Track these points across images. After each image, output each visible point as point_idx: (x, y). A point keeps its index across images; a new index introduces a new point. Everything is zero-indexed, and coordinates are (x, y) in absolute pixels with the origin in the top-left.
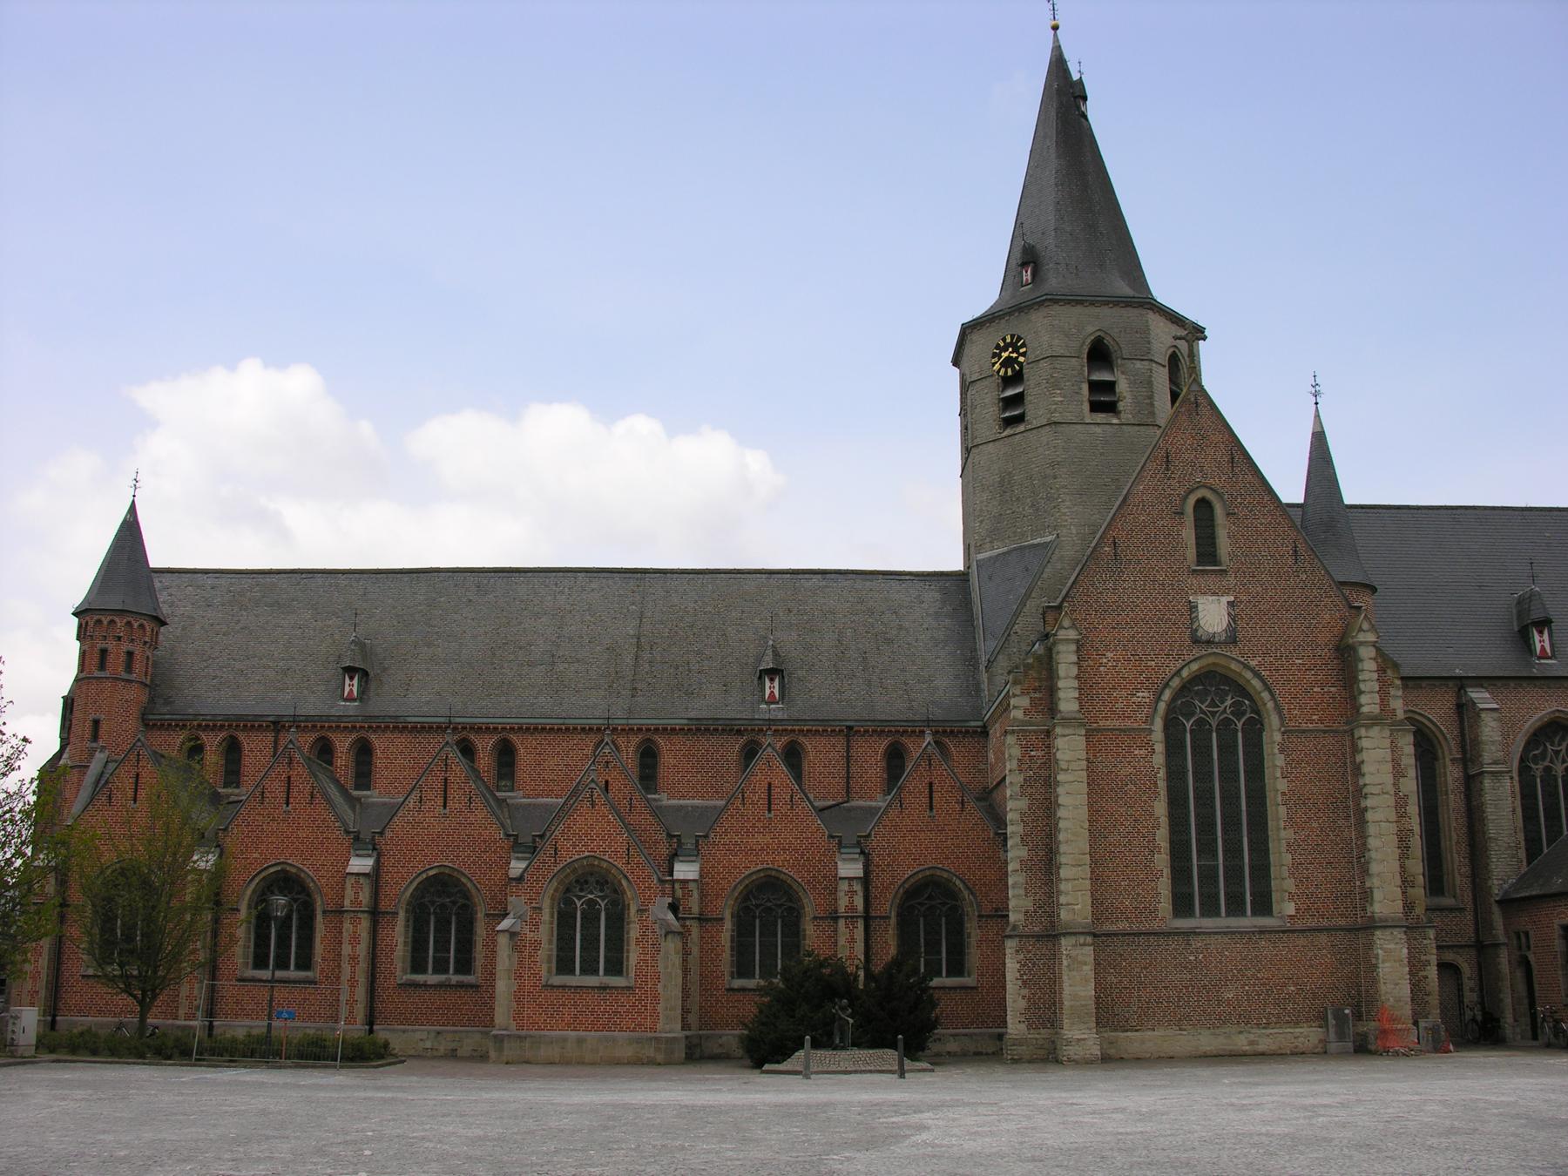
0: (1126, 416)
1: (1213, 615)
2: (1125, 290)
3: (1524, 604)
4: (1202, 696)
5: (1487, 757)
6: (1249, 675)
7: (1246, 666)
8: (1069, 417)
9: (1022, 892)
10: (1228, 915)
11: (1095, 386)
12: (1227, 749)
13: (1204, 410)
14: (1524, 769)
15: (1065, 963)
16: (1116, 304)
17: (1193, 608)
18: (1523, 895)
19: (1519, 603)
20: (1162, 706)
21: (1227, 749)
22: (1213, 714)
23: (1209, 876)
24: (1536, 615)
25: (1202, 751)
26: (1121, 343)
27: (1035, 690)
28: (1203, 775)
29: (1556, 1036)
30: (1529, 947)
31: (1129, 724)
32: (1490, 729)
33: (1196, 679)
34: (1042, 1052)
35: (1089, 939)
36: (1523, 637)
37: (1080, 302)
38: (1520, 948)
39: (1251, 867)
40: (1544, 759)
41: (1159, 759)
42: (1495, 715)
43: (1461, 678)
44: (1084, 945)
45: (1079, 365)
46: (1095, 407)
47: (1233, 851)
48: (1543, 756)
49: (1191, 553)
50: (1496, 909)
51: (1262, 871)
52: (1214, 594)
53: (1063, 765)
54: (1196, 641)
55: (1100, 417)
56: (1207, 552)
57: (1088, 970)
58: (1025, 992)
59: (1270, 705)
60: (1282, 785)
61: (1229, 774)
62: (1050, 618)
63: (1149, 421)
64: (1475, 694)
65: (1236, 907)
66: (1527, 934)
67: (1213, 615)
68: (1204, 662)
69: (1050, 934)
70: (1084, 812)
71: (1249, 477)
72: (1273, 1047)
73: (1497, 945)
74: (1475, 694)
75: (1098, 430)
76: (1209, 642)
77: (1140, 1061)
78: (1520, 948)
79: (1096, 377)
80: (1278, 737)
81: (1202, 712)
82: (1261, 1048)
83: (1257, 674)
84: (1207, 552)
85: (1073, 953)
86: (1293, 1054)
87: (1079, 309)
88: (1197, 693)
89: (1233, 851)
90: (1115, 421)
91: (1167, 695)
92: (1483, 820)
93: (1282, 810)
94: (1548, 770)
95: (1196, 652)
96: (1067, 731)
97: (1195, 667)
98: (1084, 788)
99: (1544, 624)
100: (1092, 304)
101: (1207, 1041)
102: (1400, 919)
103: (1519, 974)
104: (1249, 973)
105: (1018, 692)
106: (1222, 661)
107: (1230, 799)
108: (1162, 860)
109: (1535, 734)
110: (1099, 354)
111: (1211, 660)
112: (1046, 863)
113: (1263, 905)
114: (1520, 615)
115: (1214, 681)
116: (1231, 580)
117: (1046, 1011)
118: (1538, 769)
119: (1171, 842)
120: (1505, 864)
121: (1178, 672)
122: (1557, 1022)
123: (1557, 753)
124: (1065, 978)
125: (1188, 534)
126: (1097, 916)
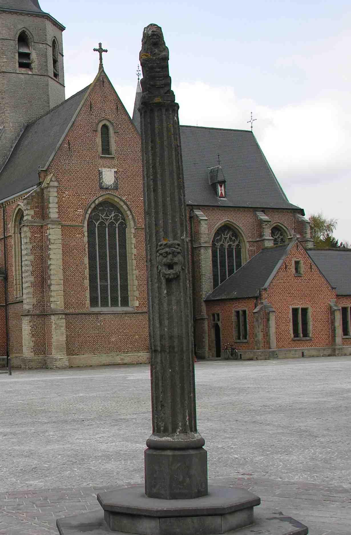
0: (35, 71)
1: (109, 177)
2: (35, 9)
3: (213, 174)
4: (102, 211)
5: (202, 240)
6: (122, 203)
7: (121, 200)
8: (9, 69)
9: (32, 296)
10: (101, 306)
11: (22, 55)
12: (112, 235)
13: (106, 85)
14: (214, 245)
15: (54, 326)
16: (32, 15)
17: (100, 173)
18: (218, 298)
19: (211, 172)
20: (87, 216)
21: (112, 235)
22: (107, 220)
23: (104, 289)
24: (220, 179)
25: (102, 236)
26: (33, 34)
27: (36, 207)
28: (102, 246)
29: (232, 355)
30: (219, 320)
31: (74, 223)
32: (204, 228)
33: (100, 204)
34: (40, 365)
35: (64, 316)
36: (214, 188)
37: (16, 13)
38: (214, 320)
39: (121, 286)
40: (221, 241)
41: (86, 239)
42: (206, 222)
43: (192, 205)
44: (62, 319)
45: (14, 43)
46: (22, 65)
47: (114, 279)
48: (220, 240)
49: (100, 149)
50: (203, 304)
51: (125, 288)
52: (109, 167)
53: (52, 241)
54: (101, 188)
55: (23, 70)
56: (106, 149)
57: (63, 329)
58: (33, 339)
59: (130, 217)
60: (135, 251)
61: (112, 247)
62: (42, 175)
63: (44, 73)
64: (198, 213)
65: (114, 303)
66: (218, 315)
67: (109, 177)
68: (104, 197)
69: (42, 314)
70: (60, 262)
71: (124, 116)
72: (130, 361)
73: (203, 319)
74: (198, 213)
75: (22, 76)
76: (107, 189)
77: (79, 367)
78: (214, 320)
79: (21, 50)
80: (133, 231)
81: (102, 219)
82: (125, 362)
83: (125, 204)
84: (106, 149)
85: (57, 322)
86: (137, 364)
87: (15, 16)
88: (100, 210)
89: (114, 279)
90: (30, 73)
91: (89, 212)
92: (199, 267)
93: (134, 262)
94: (230, 246)
95: (102, 193)
96: (53, 227)
97: (101, 199)
98: (61, 252)
99: (222, 183)
100: (21, 14)
101: (105, 359)
102: (62, 310)
103: (213, 331)
104: (121, 331)
105: (29, 208)
106: (112, 197)
107: (113, 257)
108: (87, 282)
109: (218, 230)
110: (23, 39)
111: (107, 196)
112: (42, 282)
113: (125, 302)
114: (212, 177)
115: (107, 205)
116: (116, 162)
117: (42, 345)
118: (218, 245)
119: (90, 275)
120: (207, 287)
121: (94, 202)
122: (233, 349)
123: (226, 238)
124: (53, 332)
125: (99, 140)
126: (67, 305)
